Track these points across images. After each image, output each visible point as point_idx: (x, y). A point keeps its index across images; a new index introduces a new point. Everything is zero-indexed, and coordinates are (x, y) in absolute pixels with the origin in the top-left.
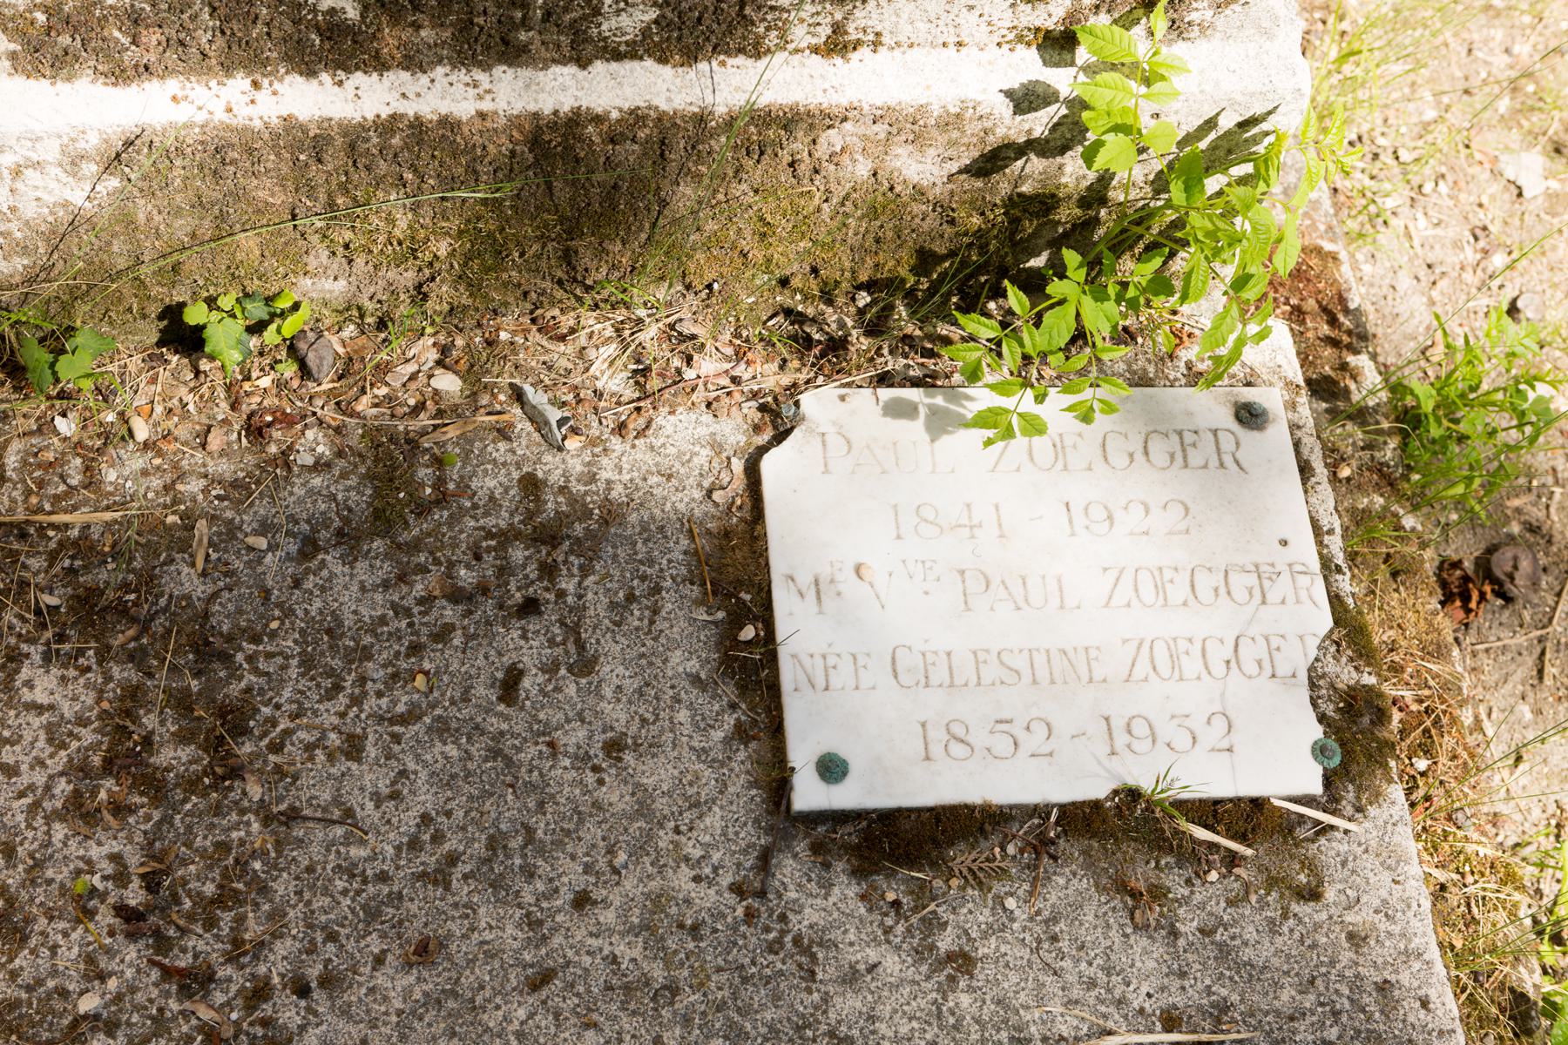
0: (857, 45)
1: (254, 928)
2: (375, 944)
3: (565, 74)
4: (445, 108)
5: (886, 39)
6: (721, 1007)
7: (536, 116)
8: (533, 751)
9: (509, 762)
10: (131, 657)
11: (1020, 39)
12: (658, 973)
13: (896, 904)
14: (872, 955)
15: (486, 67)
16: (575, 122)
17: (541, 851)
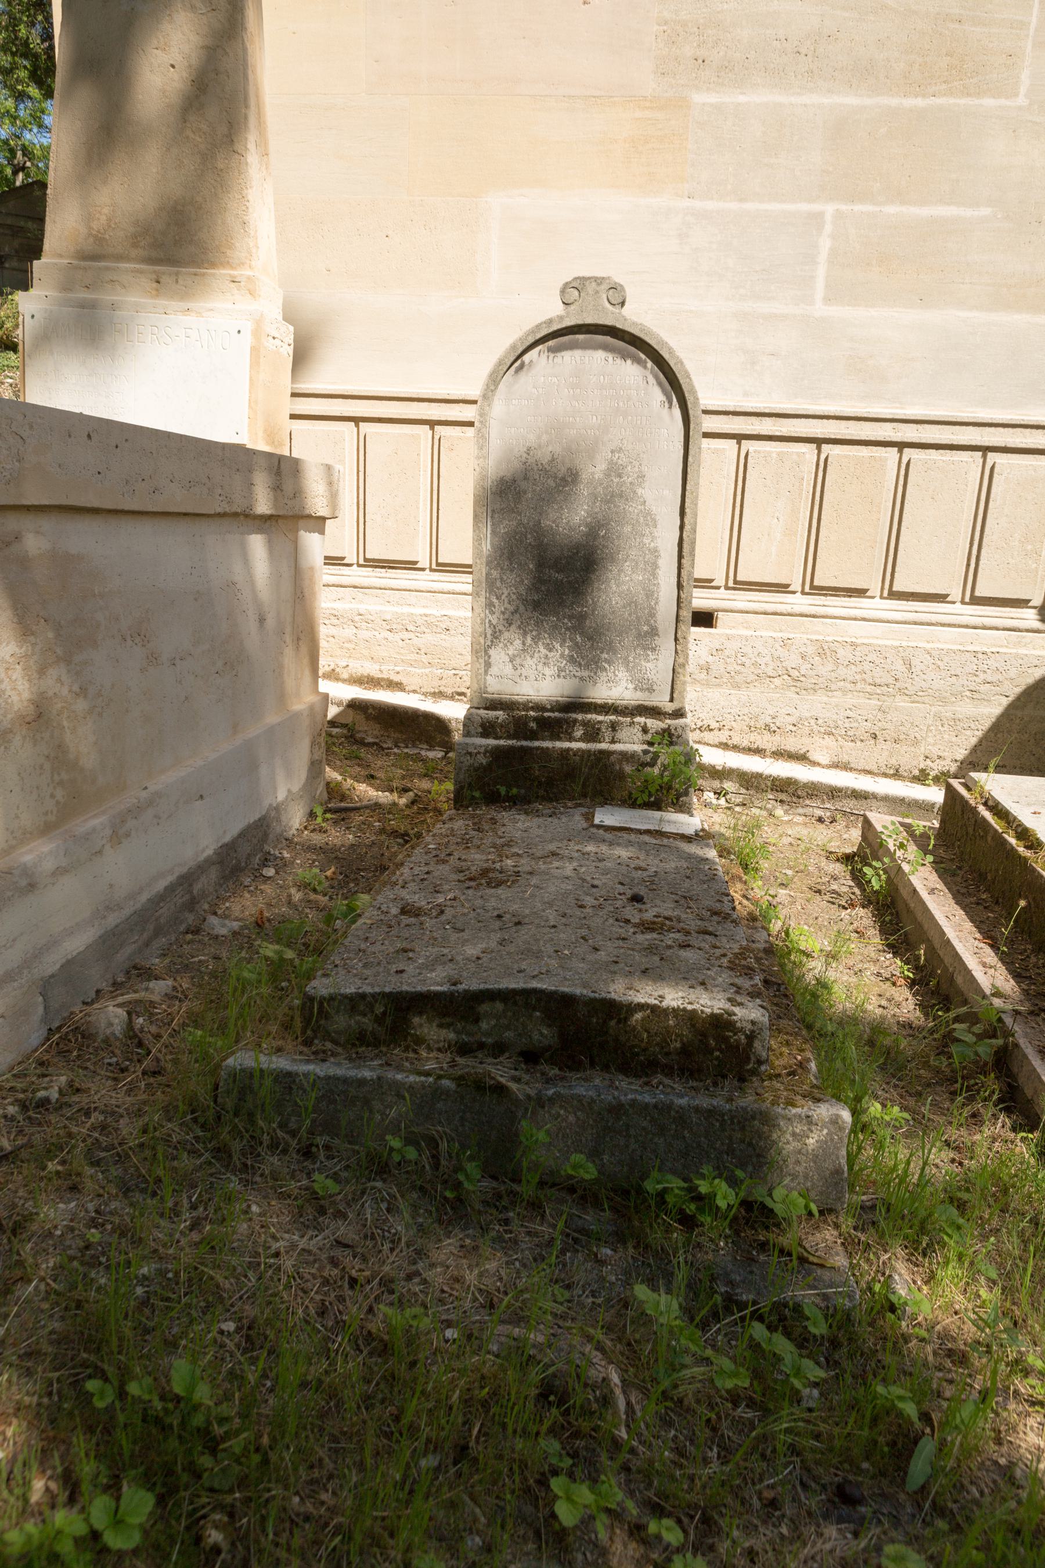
16: (569, 750)
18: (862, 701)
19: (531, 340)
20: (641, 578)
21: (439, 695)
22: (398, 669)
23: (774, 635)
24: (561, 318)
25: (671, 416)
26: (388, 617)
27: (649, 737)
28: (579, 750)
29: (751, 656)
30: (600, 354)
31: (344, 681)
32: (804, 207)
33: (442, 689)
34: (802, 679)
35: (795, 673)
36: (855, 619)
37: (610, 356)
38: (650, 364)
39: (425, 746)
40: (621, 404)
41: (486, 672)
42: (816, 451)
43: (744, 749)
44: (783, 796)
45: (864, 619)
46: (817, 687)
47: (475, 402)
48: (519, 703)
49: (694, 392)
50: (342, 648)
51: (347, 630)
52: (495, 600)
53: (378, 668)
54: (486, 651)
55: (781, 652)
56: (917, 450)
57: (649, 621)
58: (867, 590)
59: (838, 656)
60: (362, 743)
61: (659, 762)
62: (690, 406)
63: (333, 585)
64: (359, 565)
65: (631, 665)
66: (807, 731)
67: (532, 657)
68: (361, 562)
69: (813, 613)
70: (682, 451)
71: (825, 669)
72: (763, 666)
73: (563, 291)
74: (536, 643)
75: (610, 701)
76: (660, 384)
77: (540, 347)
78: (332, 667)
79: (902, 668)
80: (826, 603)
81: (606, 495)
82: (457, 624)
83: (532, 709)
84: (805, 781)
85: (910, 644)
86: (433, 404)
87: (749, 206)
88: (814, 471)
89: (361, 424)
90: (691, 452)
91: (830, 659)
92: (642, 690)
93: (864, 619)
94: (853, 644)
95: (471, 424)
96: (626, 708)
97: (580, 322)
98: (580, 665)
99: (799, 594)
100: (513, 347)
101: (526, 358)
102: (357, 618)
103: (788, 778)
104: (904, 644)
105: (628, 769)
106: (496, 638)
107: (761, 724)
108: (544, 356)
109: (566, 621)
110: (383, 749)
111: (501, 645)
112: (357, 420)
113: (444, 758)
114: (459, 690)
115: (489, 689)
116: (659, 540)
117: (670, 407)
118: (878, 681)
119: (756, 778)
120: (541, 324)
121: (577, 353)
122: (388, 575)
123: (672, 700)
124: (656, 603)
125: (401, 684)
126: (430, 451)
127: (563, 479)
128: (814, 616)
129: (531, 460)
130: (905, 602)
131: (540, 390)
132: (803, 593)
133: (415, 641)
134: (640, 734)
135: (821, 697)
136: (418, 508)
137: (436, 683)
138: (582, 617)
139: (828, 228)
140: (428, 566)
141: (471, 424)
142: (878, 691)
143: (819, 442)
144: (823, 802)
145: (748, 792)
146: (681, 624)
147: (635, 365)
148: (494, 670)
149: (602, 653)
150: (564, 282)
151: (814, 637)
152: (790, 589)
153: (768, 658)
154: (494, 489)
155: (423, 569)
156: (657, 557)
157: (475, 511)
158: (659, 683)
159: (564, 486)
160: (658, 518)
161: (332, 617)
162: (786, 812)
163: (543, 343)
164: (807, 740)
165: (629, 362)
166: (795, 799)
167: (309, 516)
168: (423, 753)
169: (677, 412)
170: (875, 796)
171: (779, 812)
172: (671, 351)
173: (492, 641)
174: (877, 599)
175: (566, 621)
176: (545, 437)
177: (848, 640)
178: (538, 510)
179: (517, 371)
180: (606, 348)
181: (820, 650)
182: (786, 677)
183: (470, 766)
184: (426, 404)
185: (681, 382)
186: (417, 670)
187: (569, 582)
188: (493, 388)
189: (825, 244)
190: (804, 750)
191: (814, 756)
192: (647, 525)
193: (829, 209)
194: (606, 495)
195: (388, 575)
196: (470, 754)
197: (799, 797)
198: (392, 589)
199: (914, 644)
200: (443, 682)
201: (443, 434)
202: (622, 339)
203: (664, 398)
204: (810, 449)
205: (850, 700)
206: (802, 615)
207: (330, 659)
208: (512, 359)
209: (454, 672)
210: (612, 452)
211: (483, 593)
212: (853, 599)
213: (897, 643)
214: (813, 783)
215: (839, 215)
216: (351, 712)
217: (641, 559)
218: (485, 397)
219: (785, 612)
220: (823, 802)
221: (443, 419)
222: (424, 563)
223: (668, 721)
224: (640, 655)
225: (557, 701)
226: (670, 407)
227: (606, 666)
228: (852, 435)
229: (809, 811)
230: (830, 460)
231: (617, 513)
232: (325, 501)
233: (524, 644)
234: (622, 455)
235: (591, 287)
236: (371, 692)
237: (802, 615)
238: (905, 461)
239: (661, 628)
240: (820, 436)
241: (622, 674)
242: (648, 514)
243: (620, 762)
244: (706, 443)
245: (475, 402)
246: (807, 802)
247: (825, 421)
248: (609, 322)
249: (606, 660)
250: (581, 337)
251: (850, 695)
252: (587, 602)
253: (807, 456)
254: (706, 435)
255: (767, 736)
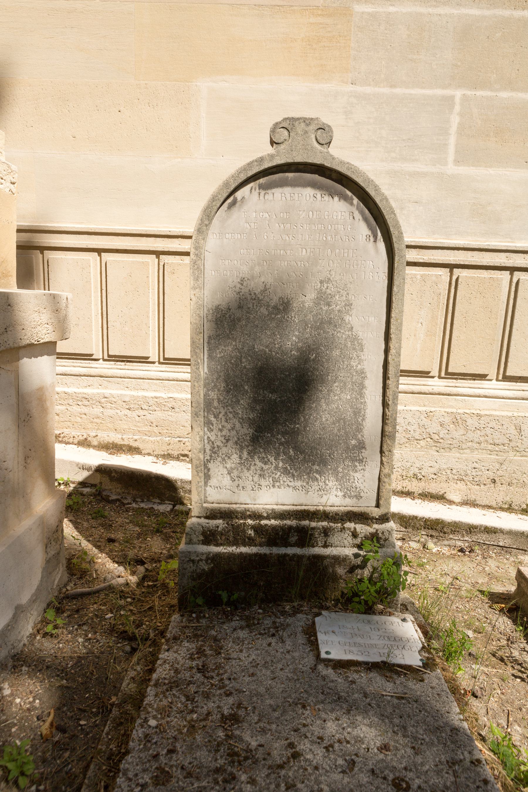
0: (329, 546)
1: (221, 672)
2: (243, 674)
3: (284, 548)
4: (265, 552)
5: (333, 545)
6: (307, 682)
7: (279, 554)
8: (273, 652)
9: (269, 653)
10: (202, 641)
11: (354, 546)
12: (296, 677)
13: (340, 673)
14: (336, 679)
15: (272, 547)
16: (286, 555)
17: (274, 663)
18: (485, 456)
19: (243, 177)
20: (349, 397)
21: (167, 457)
22: (135, 437)
23: (420, 409)
24: (272, 156)
25: (377, 249)
26: (127, 399)
27: (358, 541)
28: (294, 555)
29: (403, 425)
30: (309, 191)
31: (94, 447)
32: (439, 92)
33: (170, 452)
34: (441, 441)
35: (436, 437)
36: (479, 396)
37: (318, 194)
38: (356, 201)
39: (157, 501)
40: (329, 238)
41: (206, 484)
42: (449, 274)
43: (398, 492)
44: (431, 532)
45: (486, 397)
46: (452, 446)
47: (190, 237)
48: (237, 512)
49: (398, 226)
50: (92, 422)
51: (95, 409)
52: (213, 419)
53: (120, 437)
54: (205, 465)
55: (425, 421)
56: (524, 273)
57: (356, 436)
58: (487, 375)
59: (468, 424)
60: (107, 500)
61: (369, 564)
62: (394, 240)
63: (84, 375)
64: (104, 360)
65: (340, 475)
66: (444, 478)
67: (248, 469)
68: (106, 357)
69: (448, 392)
70: (386, 282)
71: (458, 433)
72: (412, 432)
73: (273, 131)
74: (252, 457)
75: (321, 508)
76: (365, 220)
77: (252, 184)
78: (85, 437)
79: (514, 432)
80: (457, 385)
81: (316, 322)
82: (180, 404)
83: (250, 517)
84: (450, 521)
85: (520, 414)
86: (158, 239)
87: (398, 91)
88: (447, 288)
89: (103, 254)
90: (396, 282)
91: (461, 426)
92: (350, 497)
93: (486, 397)
94: (478, 415)
95: (187, 254)
96: (337, 514)
97: (290, 160)
98: (293, 476)
99: (436, 379)
100: (226, 184)
101: (239, 194)
102: (103, 400)
103: (437, 519)
104: (516, 414)
105: (341, 571)
106: (215, 453)
107: (411, 474)
108: (255, 193)
109: (279, 436)
110: (124, 505)
111: (219, 459)
112: (99, 251)
113: (172, 510)
114: (183, 453)
115: (209, 499)
116: (365, 363)
117: (375, 241)
118: (497, 442)
119: (412, 519)
120: (252, 162)
121: (287, 190)
122: (126, 367)
123: (378, 506)
124: (363, 420)
125: (138, 448)
126: (156, 274)
127: (275, 307)
128: (449, 395)
129: (245, 290)
130: (514, 384)
131: (252, 225)
132: (440, 377)
133: (149, 417)
134: (350, 539)
135: (455, 454)
136: (148, 317)
137: (165, 448)
138: (294, 433)
139: (457, 108)
140: (157, 360)
141: (187, 254)
142: (497, 449)
143: (451, 267)
144: (463, 536)
145: (406, 530)
146: (386, 439)
147: (342, 201)
148: (213, 482)
149: (314, 465)
150: (274, 123)
151: (449, 410)
152: (430, 375)
153: (416, 426)
154: (210, 317)
155: (153, 363)
156: (363, 378)
157: (192, 338)
158: (365, 490)
159: (277, 314)
160: (364, 342)
161: (84, 400)
162: (435, 544)
163: (255, 180)
164: (444, 485)
165: (336, 198)
166: (441, 535)
167: (31, 345)
168: (156, 507)
169: (381, 246)
170: (502, 531)
171: (431, 545)
172: (377, 188)
173: (211, 456)
174: (494, 382)
175: (279, 436)
176: (257, 269)
177: (475, 412)
178: (252, 336)
179: (231, 206)
180: (314, 185)
181: (454, 420)
182: (429, 440)
183: (193, 572)
184: (152, 239)
185: (386, 217)
186: (151, 438)
187: (282, 402)
188: (207, 222)
189: (455, 120)
190: (443, 492)
191: (450, 496)
192: (354, 349)
193: (458, 94)
194: (316, 322)
195: (126, 367)
196: (193, 561)
197: (445, 533)
198: (130, 378)
199: (523, 414)
200: (171, 447)
201: (166, 261)
202: (329, 177)
203: (370, 233)
204: (444, 273)
205: (477, 455)
206: (439, 394)
207: (83, 430)
208: (225, 195)
209: (178, 439)
210: (321, 282)
211: (202, 413)
212: (476, 381)
213: (510, 414)
214: (455, 523)
215: (465, 98)
216: (98, 475)
217: (349, 379)
218: (199, 231)
219: (427, 392)
220: (463, 536)
221: (166, 250)
222: (154, 357)
223: (376, 526)
224: (348, 466)
225: (273, 510)
226: (375, 241)
227: (318, 476)
228: (477, 262)
229: (452, 542)
230: (460, 280)
231: (326, 338)
232: (50, 327)
233: (241, 457)
234: (330, 285)
235: (300, 127)
236: (114, 457)
237: (439, 394)
238: (515, 280)
239: (367, 442)
240: (452, 263)
241: (332, 483)
242: (355, 339)
243: (333, 566)
244: (410, 271)
245: (190, 237)
246: (451, 536)
247: (456, 251)
248: (318, 161)
249: (317, 472)
250: (290, 175)
251: (476, 452)
252: (299, 419)
253: (443, 277)
254: (409, 264)
255: (415, 482)
